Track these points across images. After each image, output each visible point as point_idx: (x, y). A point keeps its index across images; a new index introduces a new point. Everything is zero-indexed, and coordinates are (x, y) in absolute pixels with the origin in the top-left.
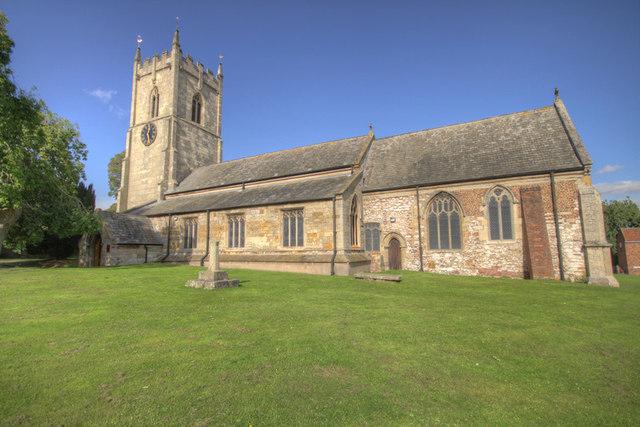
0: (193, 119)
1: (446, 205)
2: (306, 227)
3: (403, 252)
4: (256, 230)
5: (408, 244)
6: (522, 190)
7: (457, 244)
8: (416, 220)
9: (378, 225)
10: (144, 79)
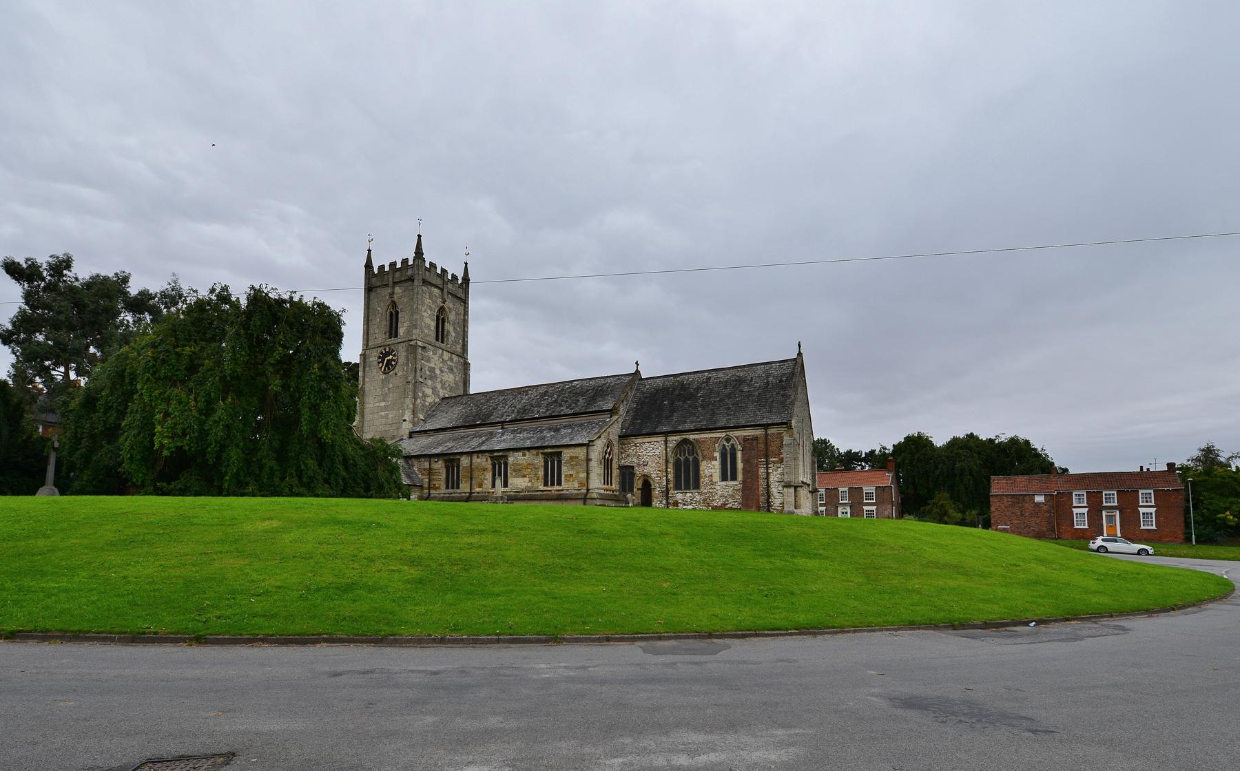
0: (437, 340)
1: (689, 449)
2: (563, 468)
3: (653, 493)
4: (519, 472)
6: (745, 439)
10: (379, 290)
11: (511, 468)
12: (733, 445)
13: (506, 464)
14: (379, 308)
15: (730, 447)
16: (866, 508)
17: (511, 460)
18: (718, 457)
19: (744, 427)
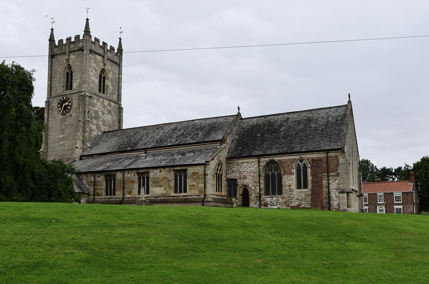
0: (100, 91)
1: (274, 167)
2: (188, 180)
3: (250, 197)
4: (157, 183)
5: (253, 192)
6: (313, 160)
7: (280, 193)
8: (258, 177)
9: (236, 180)
10: (59, 57)
11: (151, 180)
12: (305, 164)
13: (148, 178)
14: (59, 70)
15: (303, 165)
16: (396, 207)
17: (151, 175)
18: (295, 173)
19: (312, 152)
